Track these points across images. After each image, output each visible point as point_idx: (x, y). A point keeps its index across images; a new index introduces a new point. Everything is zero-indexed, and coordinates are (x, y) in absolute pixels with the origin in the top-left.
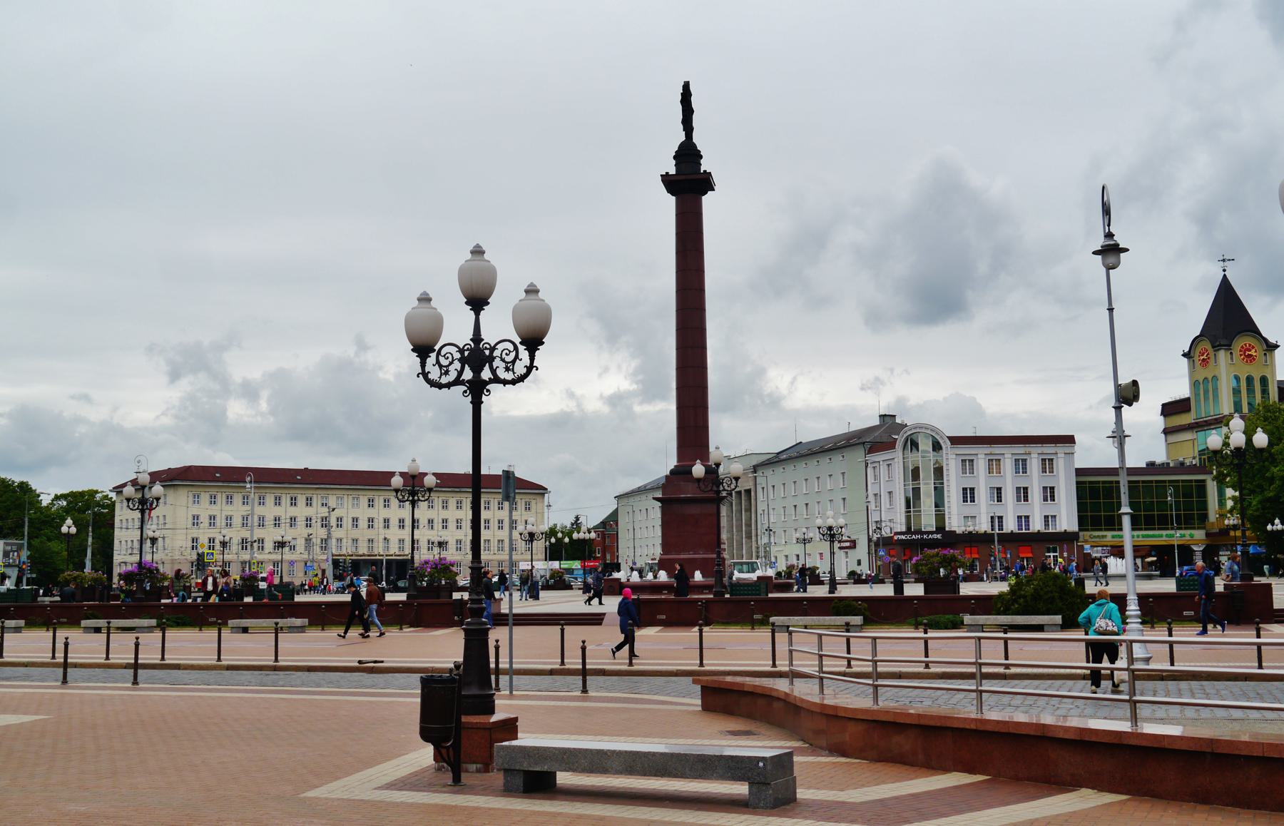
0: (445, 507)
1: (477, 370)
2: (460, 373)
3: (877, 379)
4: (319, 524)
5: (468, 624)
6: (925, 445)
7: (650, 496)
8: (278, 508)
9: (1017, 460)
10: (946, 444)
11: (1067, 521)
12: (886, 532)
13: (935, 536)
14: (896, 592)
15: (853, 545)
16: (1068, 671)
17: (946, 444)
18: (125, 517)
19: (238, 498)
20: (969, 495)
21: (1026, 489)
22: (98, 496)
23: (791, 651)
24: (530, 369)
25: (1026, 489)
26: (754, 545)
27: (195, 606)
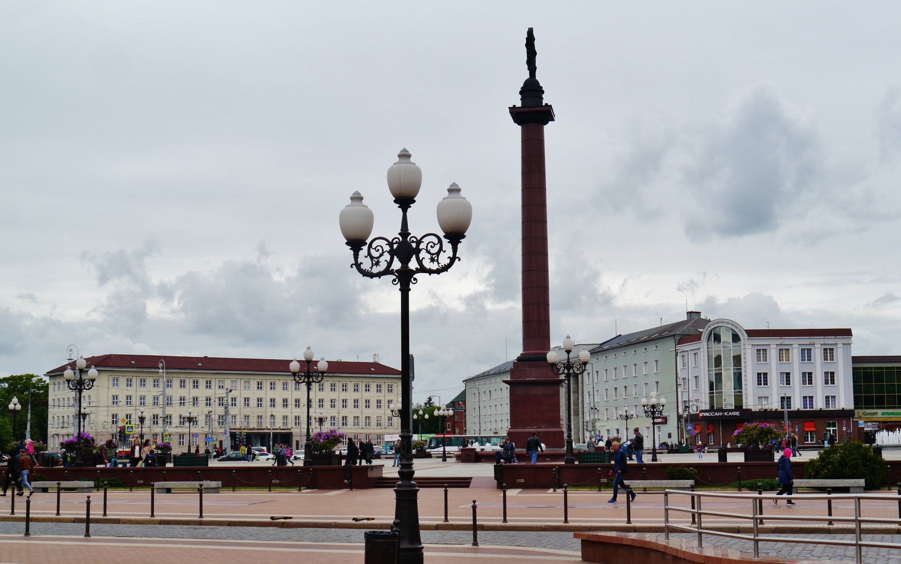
0: (345, 389)
1: (405, 261)
2: (390, 264)
3: (692, 282)
4: (217, 403)
5: (399, 486)
6: (726, 337)
7: (499, 379)
8: (182, 390)
9: (825, 350)
10: (743, 336)
11: (845, 400)
12: (693, 410)
13: (734, 413)
14: (410, 466)
15: (665, 421)
16: (884, 526)
17: (743, 336)
18: (60, 400)
19: (149, 382)
20: (762, 379)
21: (810, 374)
22: (34, 380)
23: (667, 510)
24: (453, 260)
25: (810, 374)
26: (581, 420)
27: (125, 471)
